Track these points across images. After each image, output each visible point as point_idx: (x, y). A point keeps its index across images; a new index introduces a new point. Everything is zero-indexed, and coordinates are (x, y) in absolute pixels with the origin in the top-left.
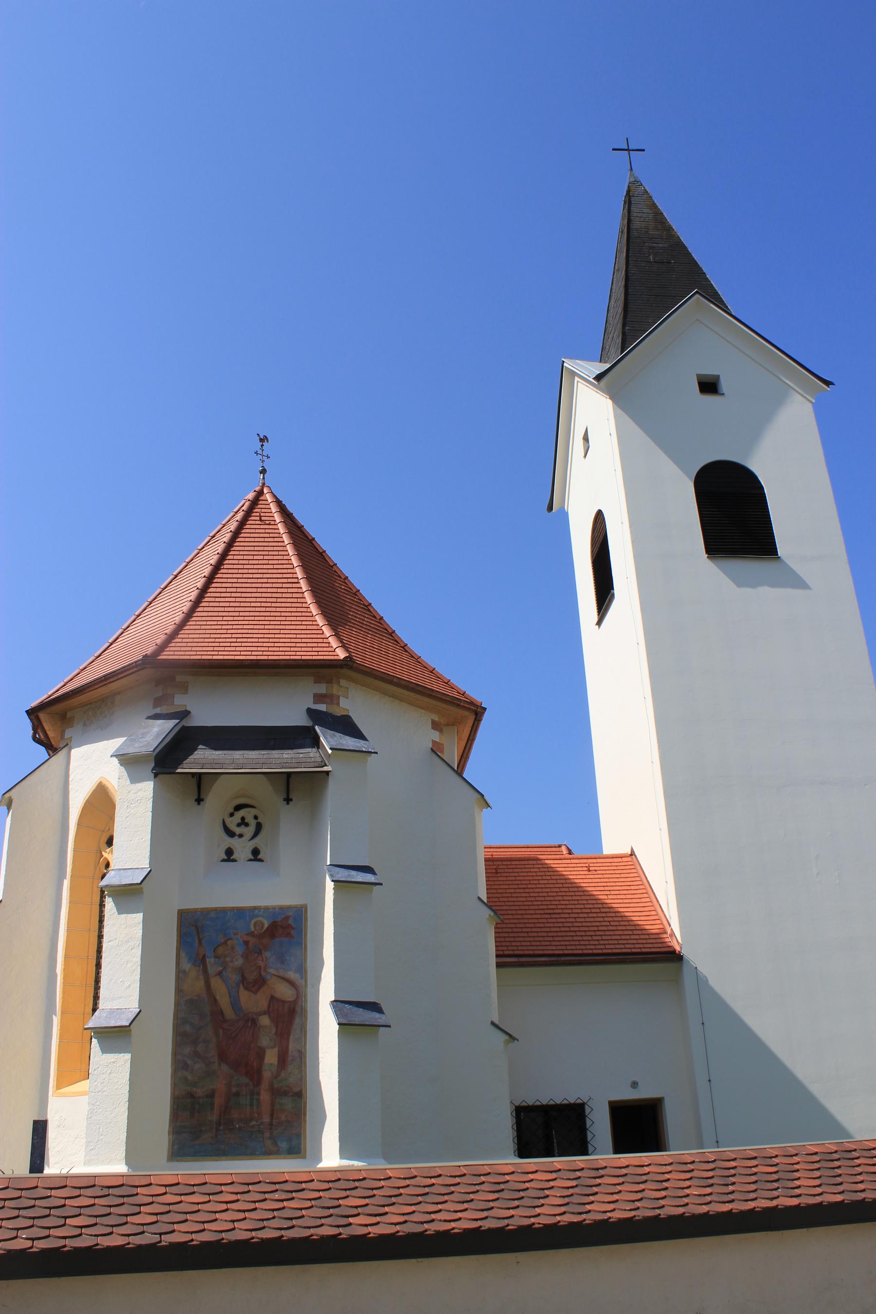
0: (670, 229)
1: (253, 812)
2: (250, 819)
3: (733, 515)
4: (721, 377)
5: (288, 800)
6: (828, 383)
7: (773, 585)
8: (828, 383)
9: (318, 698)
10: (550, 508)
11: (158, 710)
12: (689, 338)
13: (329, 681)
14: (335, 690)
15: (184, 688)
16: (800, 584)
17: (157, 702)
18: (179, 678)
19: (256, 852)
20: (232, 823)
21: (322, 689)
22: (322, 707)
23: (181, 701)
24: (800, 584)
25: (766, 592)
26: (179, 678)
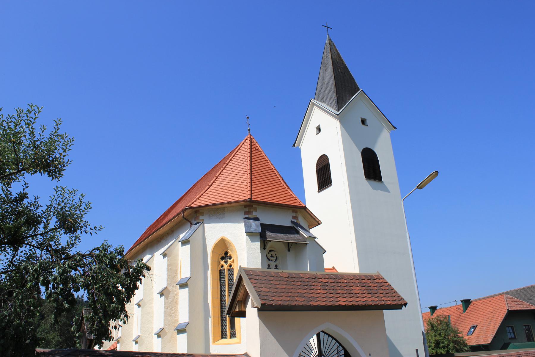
0: (342, 61)
1: (275, 253)
2: (274, 255)
3: (371, 167)
4: (367, 120)
5: (289, 250)
6: (395, 128)
7: (381, 190)
8: (395, 128)
9: (294, 217)
10: (294, 145)
11: (247, 216)
12: (357, 105)
13: (296, 212)
14: (252, 210)
15: (256, 210)
16: (387, 190)
17: (246, 213)
18: (254, 206)
19: (276, 266)
20: (269, 256)
21: (294, 214)
22: (295, 221)
23: (255, 214)
24: (387, 190)
25: (379, 192)
26: (254, 206)
